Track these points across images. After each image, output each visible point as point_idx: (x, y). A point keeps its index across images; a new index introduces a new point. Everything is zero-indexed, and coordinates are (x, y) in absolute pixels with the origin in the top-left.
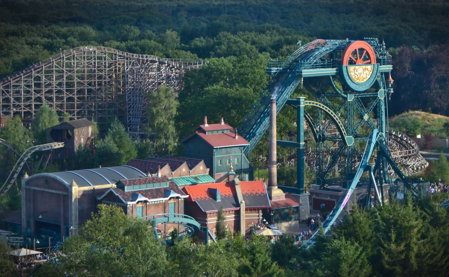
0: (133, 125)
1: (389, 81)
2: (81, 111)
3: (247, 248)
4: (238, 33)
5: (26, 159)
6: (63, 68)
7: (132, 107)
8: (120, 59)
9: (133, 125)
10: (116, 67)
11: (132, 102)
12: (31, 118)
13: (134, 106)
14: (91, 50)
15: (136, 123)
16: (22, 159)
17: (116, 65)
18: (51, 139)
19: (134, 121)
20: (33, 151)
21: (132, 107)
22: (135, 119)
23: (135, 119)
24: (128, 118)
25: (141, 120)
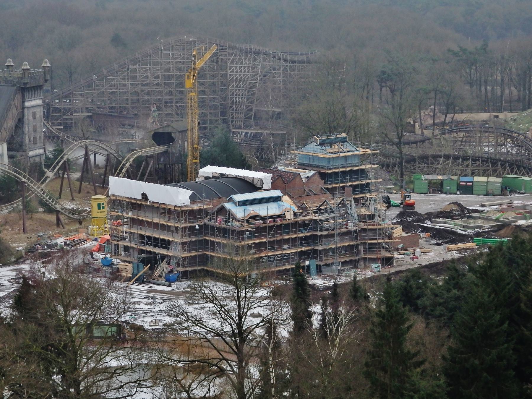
0: (236, 122)
1: (217, 150)
2: (357, 245)
3: (454, 346)
4: (4, 395)
5: (127, 165)
6: (161, 60)
7: (235, 101)
8: (222, 49)
9: (236, 122)
10: (217, 58)
11: (235, 96)
12: (127, 113)
13: (237, 101)
14: (191, 40)
15: (239, 119)
16: (124, 165)
17: (217, 56)
18: (154, 142)
19: (238, 109)
20: (135, 156)
21: (235, 101)
22: (238, 114)
23: (238, 114)
24: (230, 114)
25: (245, 116)
